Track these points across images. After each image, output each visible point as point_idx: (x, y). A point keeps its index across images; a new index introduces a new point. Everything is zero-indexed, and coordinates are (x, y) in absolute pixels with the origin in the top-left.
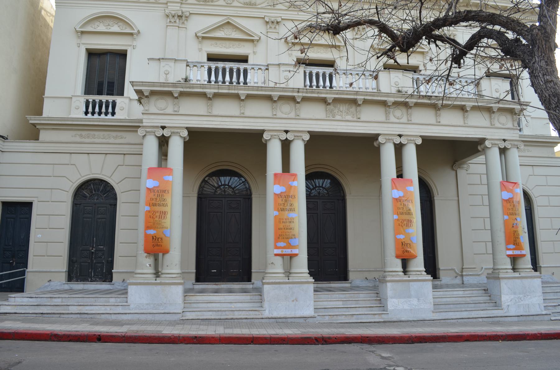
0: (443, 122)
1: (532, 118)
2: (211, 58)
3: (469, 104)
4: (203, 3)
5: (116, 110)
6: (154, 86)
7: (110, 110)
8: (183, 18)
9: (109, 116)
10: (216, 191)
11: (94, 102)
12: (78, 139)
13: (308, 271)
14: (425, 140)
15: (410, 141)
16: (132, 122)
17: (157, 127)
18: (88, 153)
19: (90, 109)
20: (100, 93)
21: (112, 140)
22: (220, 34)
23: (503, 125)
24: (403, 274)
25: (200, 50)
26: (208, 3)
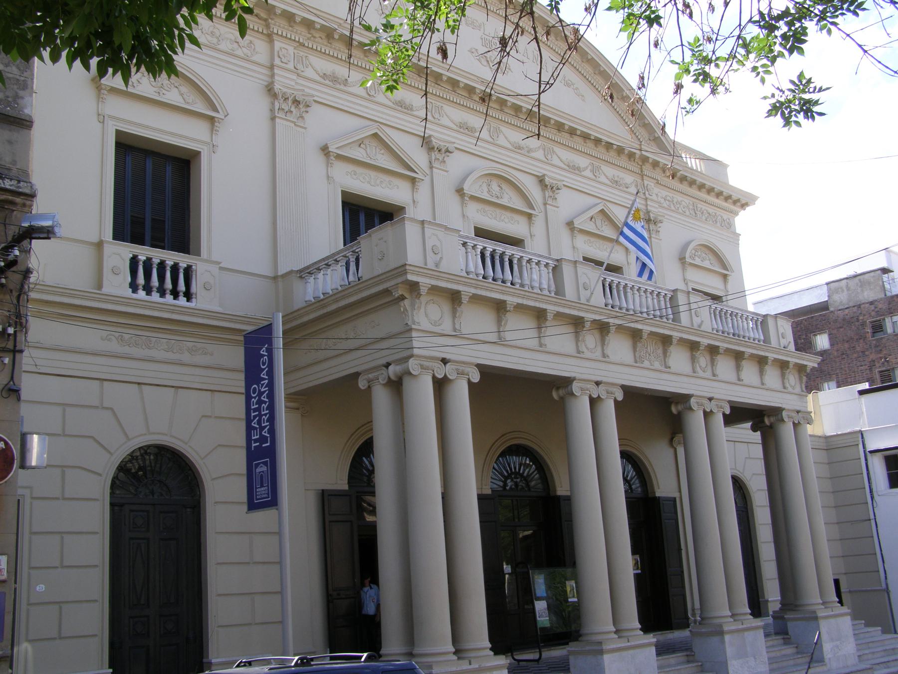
0: (613, 358)
1: (221, 268)
2: (480, 233)
3: (467, 291)
4: (330, 83)
5: (193, 289)
6: (438, 278)
7: (182, 287)
8: (301, 106)
9: (182, 301)
10: (505, 485)
11: (148, 263)
12: (114, 346)
13: (490, 646)
14: (627, 390)
15: (461, 373)
16: (209, 318)
17: (432, 358)
18: (139, 384)
19: (141, 280)
20: (157, 243)
21: (186, 357)
22: (358, 154)
23: (435, 324)
24: (455, 658)
25: (102, 119)
26: (338, 86)
